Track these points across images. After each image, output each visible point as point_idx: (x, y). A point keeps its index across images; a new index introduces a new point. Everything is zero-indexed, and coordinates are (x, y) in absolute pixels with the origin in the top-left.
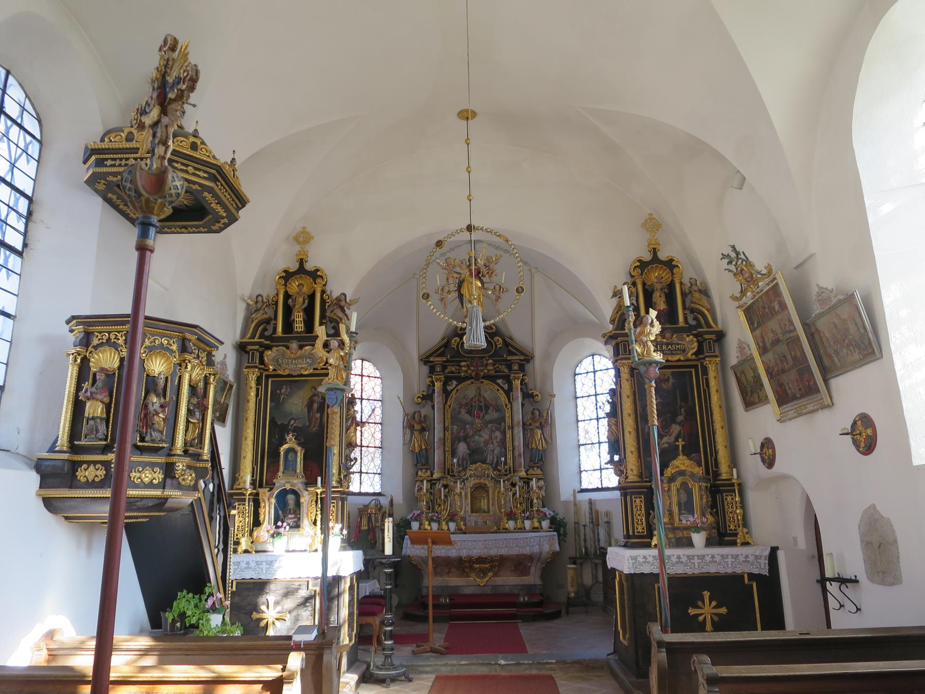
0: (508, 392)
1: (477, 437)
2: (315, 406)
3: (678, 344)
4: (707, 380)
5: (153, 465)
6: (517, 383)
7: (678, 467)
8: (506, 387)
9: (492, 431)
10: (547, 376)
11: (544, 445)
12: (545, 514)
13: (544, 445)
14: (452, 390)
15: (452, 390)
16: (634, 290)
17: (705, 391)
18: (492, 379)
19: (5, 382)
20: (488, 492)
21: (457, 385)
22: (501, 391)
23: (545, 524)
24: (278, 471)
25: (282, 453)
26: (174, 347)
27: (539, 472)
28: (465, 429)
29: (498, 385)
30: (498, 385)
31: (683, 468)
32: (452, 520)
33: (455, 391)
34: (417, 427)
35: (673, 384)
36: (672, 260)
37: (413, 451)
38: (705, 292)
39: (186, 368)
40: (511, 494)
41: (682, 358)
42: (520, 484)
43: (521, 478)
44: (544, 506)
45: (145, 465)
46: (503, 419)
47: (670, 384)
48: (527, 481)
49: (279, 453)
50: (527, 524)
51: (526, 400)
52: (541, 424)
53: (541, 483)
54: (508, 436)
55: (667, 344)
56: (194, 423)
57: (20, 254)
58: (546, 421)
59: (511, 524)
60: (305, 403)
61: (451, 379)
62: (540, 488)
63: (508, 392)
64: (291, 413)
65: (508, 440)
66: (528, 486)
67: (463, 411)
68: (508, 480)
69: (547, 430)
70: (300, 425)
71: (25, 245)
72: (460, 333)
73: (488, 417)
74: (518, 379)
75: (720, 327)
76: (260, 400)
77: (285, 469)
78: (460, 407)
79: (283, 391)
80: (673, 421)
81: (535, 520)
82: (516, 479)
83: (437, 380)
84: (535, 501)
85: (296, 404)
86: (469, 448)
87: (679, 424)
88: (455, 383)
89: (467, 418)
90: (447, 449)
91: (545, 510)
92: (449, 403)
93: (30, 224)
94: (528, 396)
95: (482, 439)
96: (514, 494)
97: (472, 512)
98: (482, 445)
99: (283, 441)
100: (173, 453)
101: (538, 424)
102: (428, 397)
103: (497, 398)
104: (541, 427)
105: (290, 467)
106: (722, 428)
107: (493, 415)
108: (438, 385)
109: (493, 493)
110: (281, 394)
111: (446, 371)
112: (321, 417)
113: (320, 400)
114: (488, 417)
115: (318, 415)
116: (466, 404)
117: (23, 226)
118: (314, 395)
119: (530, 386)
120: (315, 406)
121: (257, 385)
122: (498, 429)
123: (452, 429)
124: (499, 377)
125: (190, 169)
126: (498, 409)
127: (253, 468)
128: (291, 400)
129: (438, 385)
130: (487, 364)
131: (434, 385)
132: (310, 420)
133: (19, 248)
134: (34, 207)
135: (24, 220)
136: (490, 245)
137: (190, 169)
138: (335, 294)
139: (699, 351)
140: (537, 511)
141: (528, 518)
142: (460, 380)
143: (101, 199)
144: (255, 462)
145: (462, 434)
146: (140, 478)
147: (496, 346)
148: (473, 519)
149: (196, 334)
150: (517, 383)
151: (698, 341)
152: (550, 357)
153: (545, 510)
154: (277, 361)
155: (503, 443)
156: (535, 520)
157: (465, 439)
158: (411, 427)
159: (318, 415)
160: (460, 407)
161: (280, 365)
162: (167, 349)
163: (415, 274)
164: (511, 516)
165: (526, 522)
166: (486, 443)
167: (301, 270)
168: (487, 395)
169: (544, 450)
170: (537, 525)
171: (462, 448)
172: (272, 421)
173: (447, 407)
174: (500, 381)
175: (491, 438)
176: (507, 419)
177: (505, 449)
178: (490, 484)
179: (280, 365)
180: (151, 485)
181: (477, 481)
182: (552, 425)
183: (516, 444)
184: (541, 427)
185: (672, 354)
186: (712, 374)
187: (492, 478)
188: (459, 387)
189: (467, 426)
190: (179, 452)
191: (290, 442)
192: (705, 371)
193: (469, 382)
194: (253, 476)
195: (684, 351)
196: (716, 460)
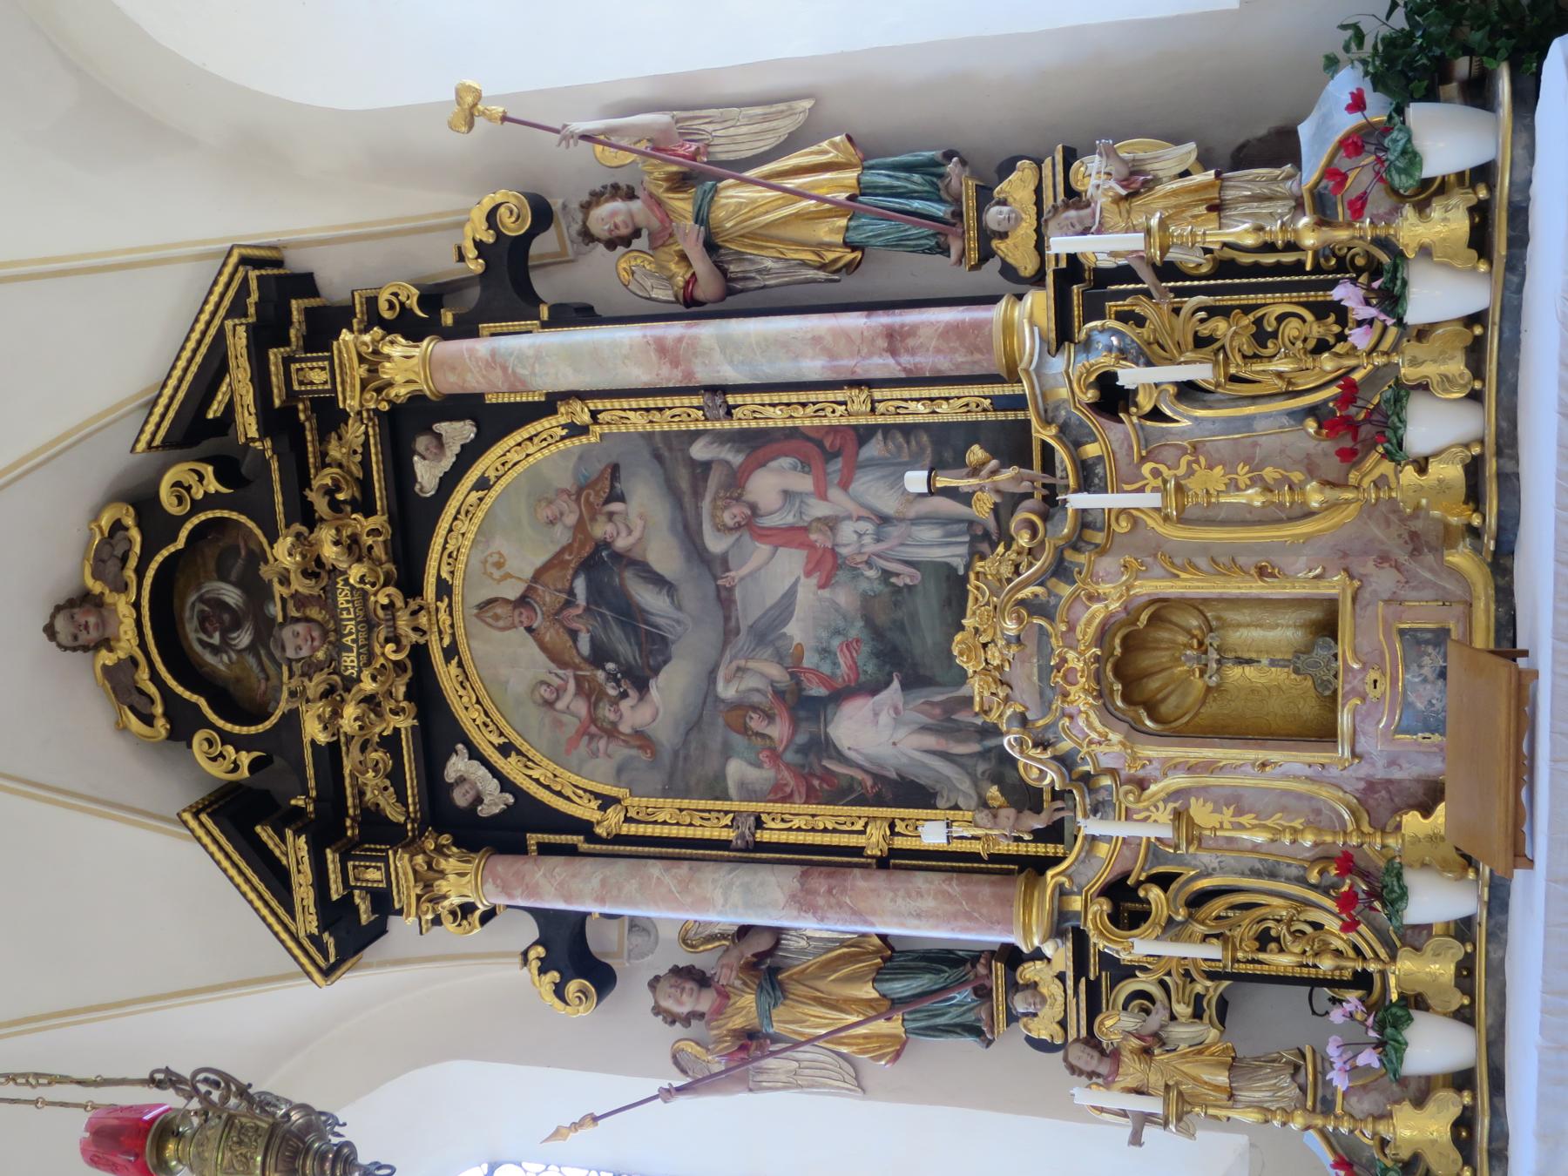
0: (495, 420)
1: (795, 631)
6: (408, 365)
8: (458, 433)
9: (751, 524)
10: (385, 151)
11: (826, 150)
12: (1353, 144)
13: (826, 150)
14: (506, 784)
15: (506, 784)
18: (412, 524)
20: (1162, 609)
21: (475, 754)
22: (486, 464)
23: (1446, 139)
27: (1018, 187)
28: (741, 707)
29: (449, 482)
30: (449, 482)
32: (1385, 889)
33: (511, 767)
34: (746, 1007)
37: (897, 1050)
40: (1185, 419)
42: (1104, 336)
43: (1064, 333)
44: (1280, 147)
46: (666, 450)
48: (1081, 290)
50: (1441, 295)
51: (542, 284)
52: (681, 182)
53: (1093, 174)
54: (777, 418)
58: (658, 147)
59: (1437, 427)
61: (435, 787)
62: (1136, 183)
63: (495, 420)
65: (803, 419)
66: (1125, 274)
67: (632, 714)
68: (1073, 437)
69: (733, 137)
73: (664, 555)
74: (372, 361)
78: (612, 732)
81: (1411, 230)
82: (1065, 379)
84: (1240, 231)
86: (874, 689)
88: (458, 765)
89: (671, 689)
90: (874, 840)
91: (1318, 138)
92: (585, 810)
94: (507, 280)
95: (807, 593)
96: (1188, 391)
97: (1325, 734)
98: (844, 597)
101: (682, 204)
103: (538, 491)
104: (696, 176)
107: (643, 522)
109: (1174, 561)
111: (394, 814)
114: (664, 555)
116: (589, 692)
119: (440, 263)
122: (736, 482)
123: (749, 794)
124: (401, 474)
125: (697, 822)
126: (603, 486)
130: (315, 568)
137: (697, 822)
140: (1322, 208)
141: (1391, 299)
142: (437, 731)
145: (778, 731)
147: (210, 501)
148: (1378, 735)
150: (408, 365)
152: (260, 143)
153: (1318, 138)
155: (831, 451)
156: (1411, 230)
157: (807, 705)
158: (751, 1043)
160: (612, 732)
164: (1360, 424)
165: (1416, 314)
166: (829, 565)
168: (524, 556)
169: (866, 151)
170: (1448, 222)
171: (872, 731)
173: (610, 822)
174: (427, 474)
175: (794, 535)
176: (662, 424)
177: (864, 434)
178: (1109, 590)
181: (1080, 700)
182: (686, 102)
183: (813, 367)
184: (696, 176)
187: (1060, 570)
188: (485, 741)
189: (727, 691)
193: (447, 675)
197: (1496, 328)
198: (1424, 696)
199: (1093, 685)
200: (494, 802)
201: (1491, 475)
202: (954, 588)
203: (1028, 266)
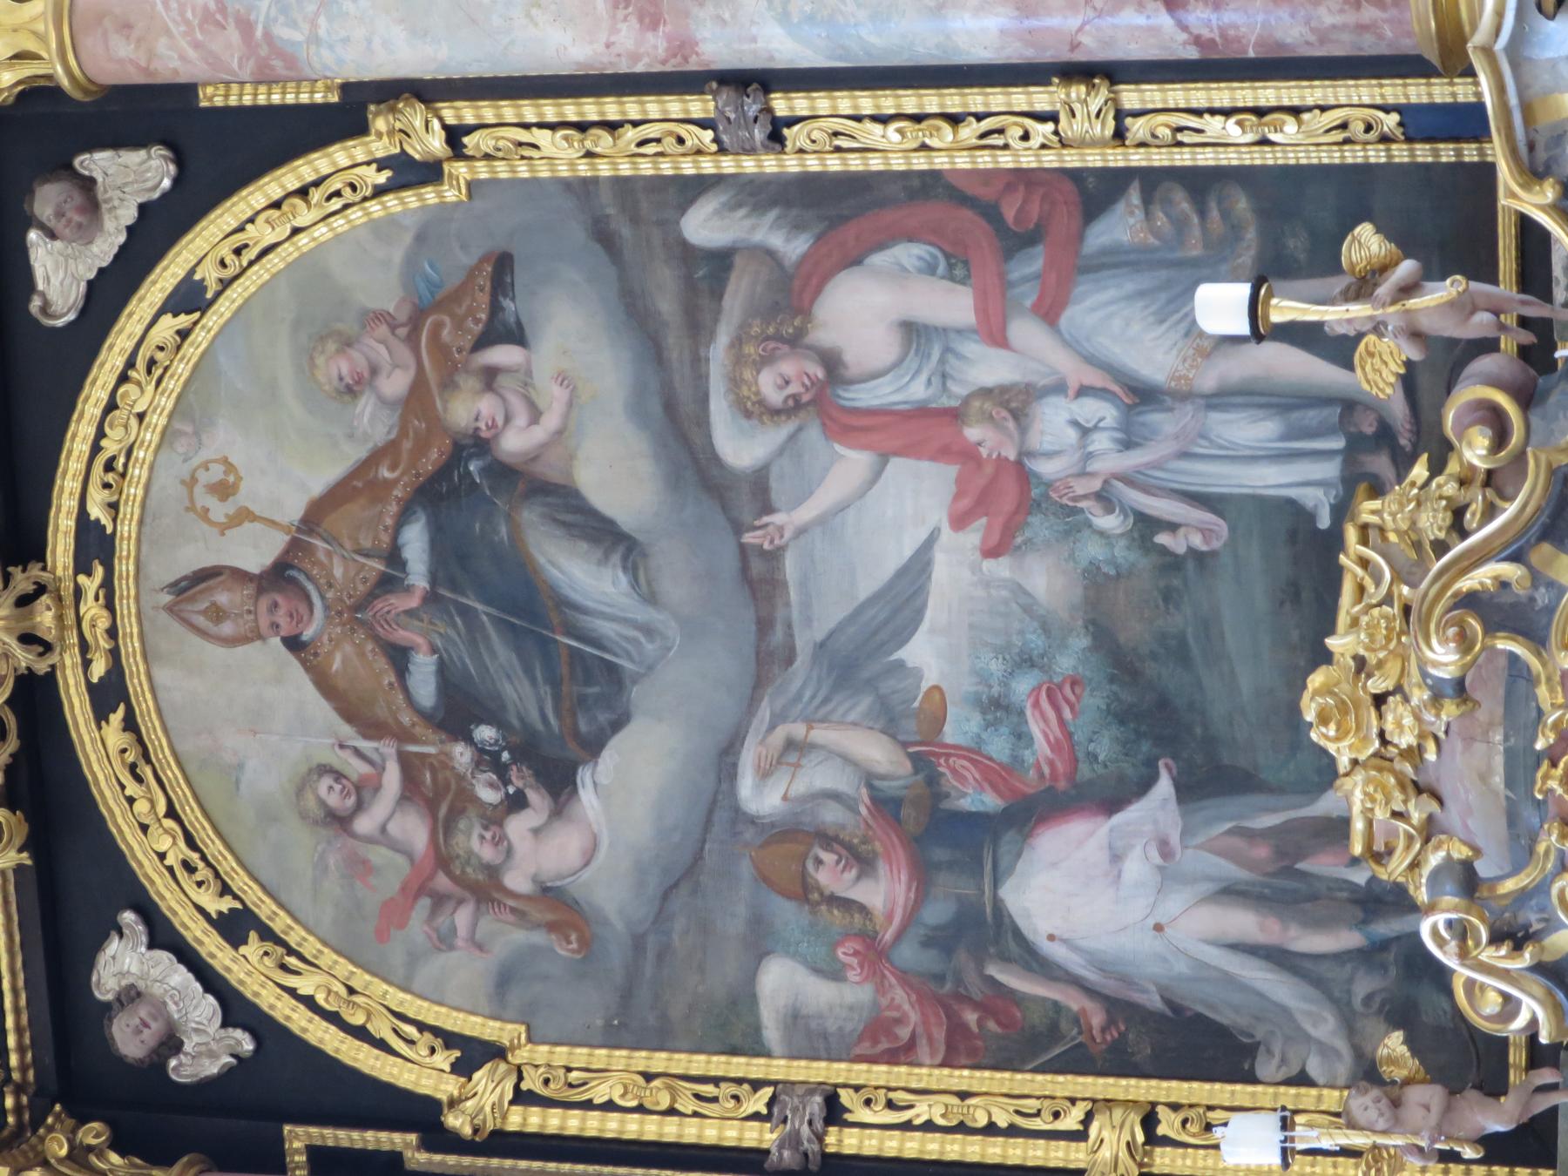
8: (133, 175)
9: (826, 403)
14: (236, 1009)
22: (197, 250)
28: (796, 835)
29: (108, 293)
30: (108, 293)
33: (247, 968)
46: (623, 224)
54: (892, 151)
65: (952, 153)
67: (536, 849)
73: (616, 472)
88: (123, 961)
95: (957, 569)
98: (1045, 578)
103: (321, 316)
107: (567, 394)
114: (616, 472)
116: (428, 790)
122: (790, 301)
123: (810, 1038)
126: (478, 303)
145: (883, 892)
157: (953, 832)
160: (486, 889)
166: (1008, 502)
168: (285, 469)
171: (1105, 895)
176: (617, 160)
177: (1098, 192)
188: (188, 906)
189: (763, 797)
193: (98, 747)
202: (1307, 563)
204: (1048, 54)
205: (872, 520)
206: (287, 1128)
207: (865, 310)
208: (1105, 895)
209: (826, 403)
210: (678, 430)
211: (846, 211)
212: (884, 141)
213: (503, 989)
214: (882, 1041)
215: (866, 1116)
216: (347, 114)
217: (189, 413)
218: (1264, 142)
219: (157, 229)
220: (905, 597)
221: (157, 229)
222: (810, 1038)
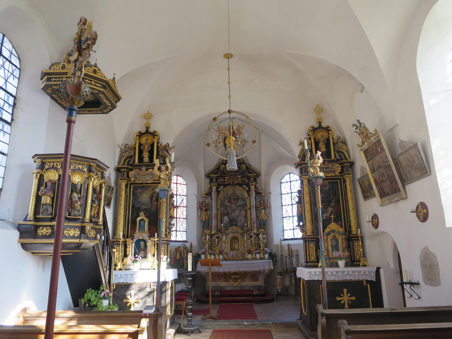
0: (248, 192)
1: (233, 214)
2: (154, 198)
3: (331, 168)
4: (345, 185)
5: (75, 227)
6: (253, 187)
7: (331, 228)
8: (247, 189)
9: (240, 211)
10: (267, 184)
11: (266, 217)
12: (266, 251)
13: (266, 217)
14: (221, 191)
15: (221, 191)
16: (310, 142)
17: (344, 191)
18: (241, 185)
19: (2, 186)
20: (238, 240)
21: (223, 188)
22: (245, 191)
23: (267, 256)
24: (136, 230)
25: (138, 221)
26: (85, 170)
28: (227, 209)
29: (243, 188)
30: (243, 188)
31: (334, 229)
32: (221, 254)
33: (222, 191)
34: (204, 209)
35: (329, 188)
36: (328, 127)
37: (202, 221)
38: (344, 143)
39: (91, 180)
40: (250, 241)
41: (333, 175)
42: (254, 236)
43: (255, 234)
44: (266, 247)
45: (71, 227)
46: (246, 205)
47: (327, 188)
48: (258, 235)
49: (137, 221)
50: (258, 256)
51: (257, 195)
52: (264, 207)
53: (265, 236)
54: (248, 213)
55: (326, 168)
56: (95, 207)
57: (10, 124)
58: (267, 205)
59: (250, 256)
60: (149, 197)
61: (220, 185)
62: (264, 238)
63: (248, 192)
64: (142, 202)
65: (248, 215)
67: (226, 201)
68: (248, 234)
69: (267, 210)
70: (147, 208)
71: (12, 120)
72: (225, 163)
73: (238, 204)
74: (253, 185)
75: (352, 160)
76: (127, 195)
77: (139, 229)
78: (225, 199)
79: (138, 191)
80: (329, 205)
81: (262, 254)
82: (252, 234)
83: (214, 186)
84: (261, 245)
85: (145, 197)
86: (229, 219)
87: (332, 207)
88: (222, 187)
90: (218, 219)
91: (266, 249)
92: (219, 197)
93: (15, 109)
94: (258, 193)
95: (236, 215)
96: (251, 241)
97: (231, 250)
98: (235, 217)
99: (138, 216)
100: (84, 221)
101: (263, 207)
102: (209, 194)
103: (243, 195)
104: (265, 208)
105: (142, 228)
106: (353, 209)
107: (241, 203)
108: (214, 188)
109: (241, 241)
110: (137, 192)
111: (218, 181)
112: (157, 204)
113: (156, 195)
114: (238, 204)
115: (155, 203)
116: (228, 197)
117: (11, 110)
118: (153, 193)
120: (154, 198)
121: (126, 188)
122: (243, 210)
123: (221, 209)
124: (244, 184)
126: (243, 200)
127: (124, 229)
128: (142, 196)
129: (214, 188)
131: (212, 188)
132: (151, 205)
133: (10, 121)
134: (16, 101)
135: (12, 108)
136: (239, 119)
138: (164, 144)
139: (342, 172)
140: (263, 249)
141: (258, 253)
142: (225, 186)
143: (49, 97)
144: (124, 226)
145: (226, 212)
146: (68, 233)
147: (242, 169)
148: (231, 253)
149: (96, 163)
150: (253, 187)
151: (341, 167)
152: (269, 174)
153: (266, 249)
154: (136, 176)
155: (246, 216)
156: (262, 254)
157: (227, 214)
158: (201, 209)
159: (155, 203)
160: (225, 199)
161: (137, 178)
162: (82, 170)
163: (203, 134)
164: (250, 252)
165: (257, 255)
166: (238, 216)
167: (147, 132)
168: (238, 193)
169: (266, 220)
170: (262, 256)
171: (226, 219)
172: (133, 206)
173: (218, 199)
174: (244, 186)
175: (240, 214)
176: (248, 205)
177: (247, 219)
178: (239, 236)
179: (137, 178)
180: (74, 237)
181: (233, 235)
182: (270, 208)
183: (252, 217)
184: (265, 208)
185: (328, 173)
186: (348, 183)
187: (241, 234)
188: (224, 189)
189: (228, 208)
190: (87, 221)
191: (142, 216)
192: (345, 181)
193: (229, 187)
194: (123, 233)
195: (334, 171)
196: (350, 225)
197: (236, 327)
198: (234, 256)
199: (347, 253)
200: (220, 190)
201: (247, 259)
202: (236, 226)
203: (259, 230)
204: (232, 269)
205: (237, 213)
206: (339, 321)
207: (243, 212)
208: (226, 219)
209: (240, 211)
210: (240, 206)
211: (246, 212)
212: (248, 212)
213: (222, 200)
214: (221, 212)
215: (249, 226)
216: (249, 196)
217: (240, 190)
218: (253, 324)
219: (246, 190)
220: (235, 213)
221: (246, 190)
222: (221, 209)
